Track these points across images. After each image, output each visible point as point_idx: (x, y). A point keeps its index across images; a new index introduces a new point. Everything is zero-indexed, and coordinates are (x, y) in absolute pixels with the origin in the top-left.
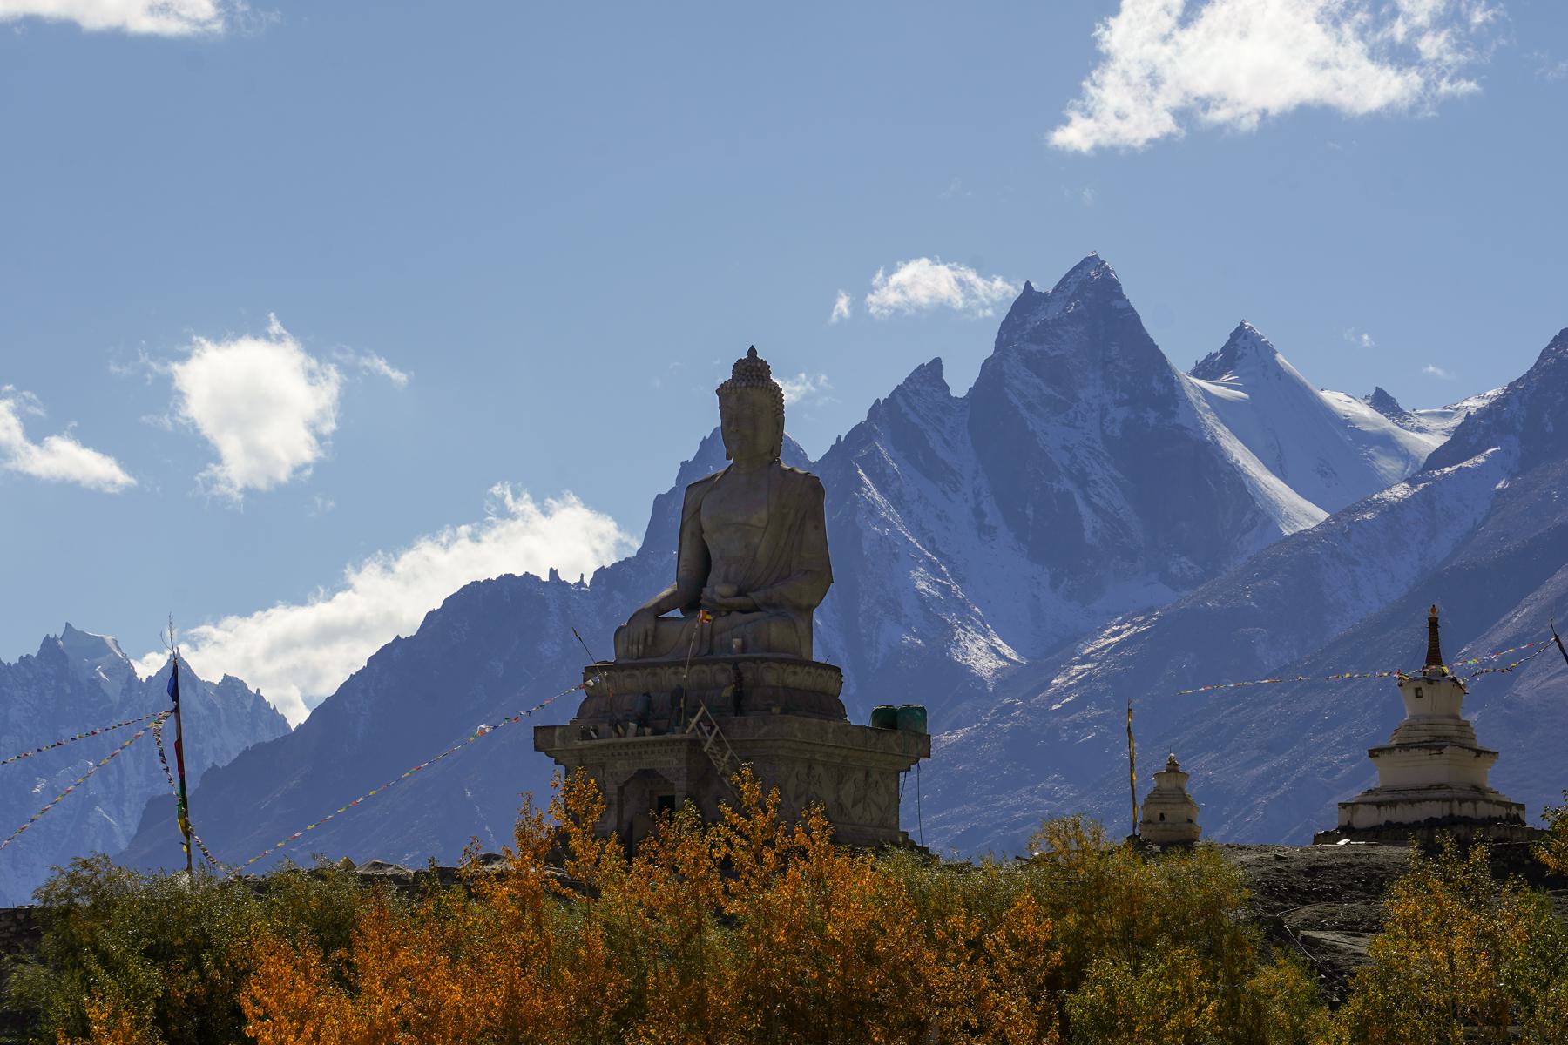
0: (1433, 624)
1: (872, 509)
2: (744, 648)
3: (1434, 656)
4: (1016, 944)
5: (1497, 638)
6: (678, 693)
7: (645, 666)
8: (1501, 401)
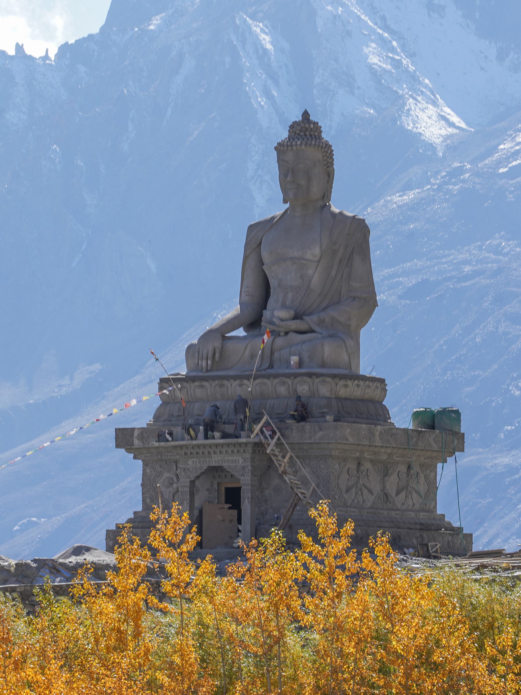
2: (300, 364)
6: (242, 404)
7: (214, 378)
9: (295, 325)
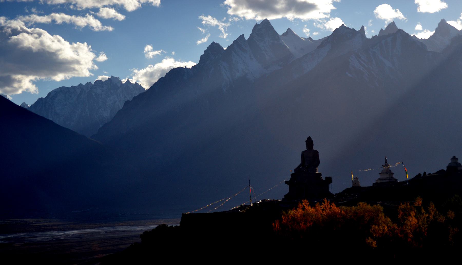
3: (386, 162)
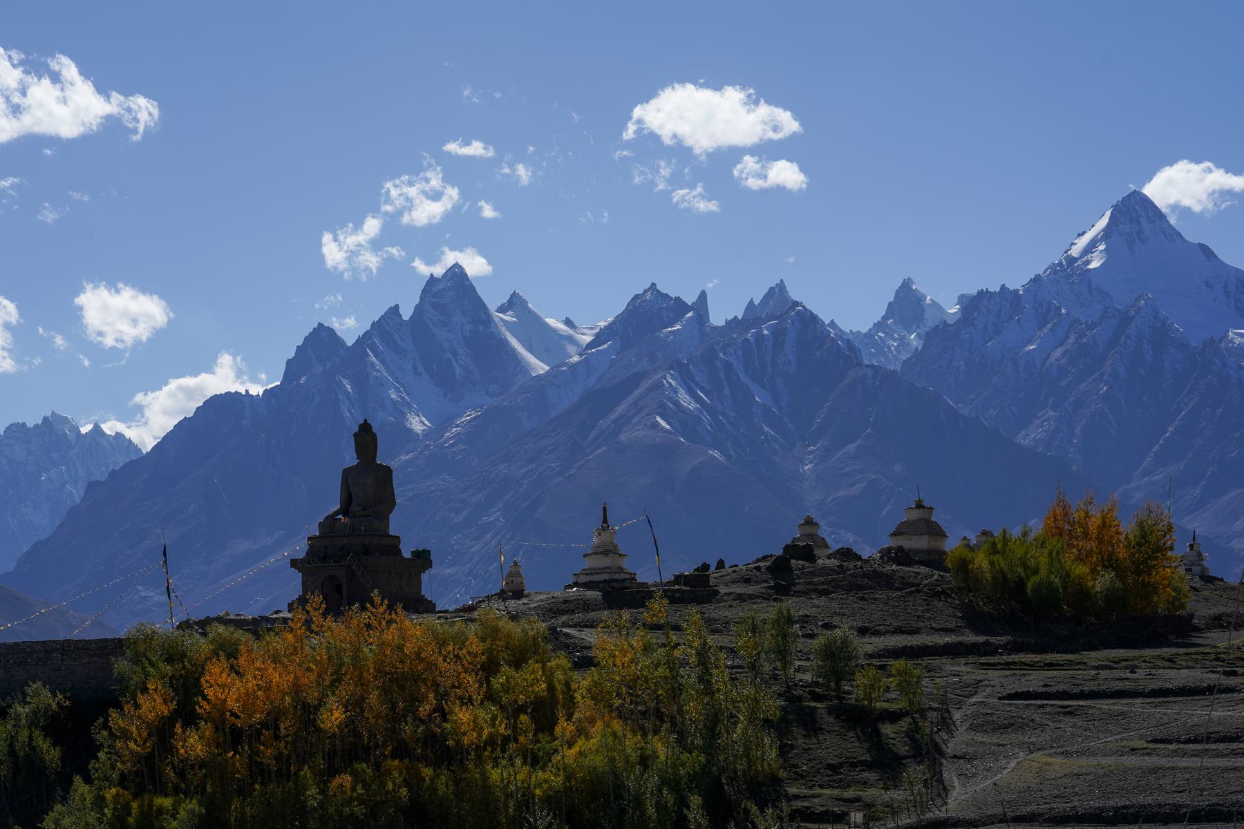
0: (605, 509)
1: (373, 365)
3: (605, 521)
4: (469, 653)
5: (613, 417)
8: (613, 323)
9: (363, 513)
